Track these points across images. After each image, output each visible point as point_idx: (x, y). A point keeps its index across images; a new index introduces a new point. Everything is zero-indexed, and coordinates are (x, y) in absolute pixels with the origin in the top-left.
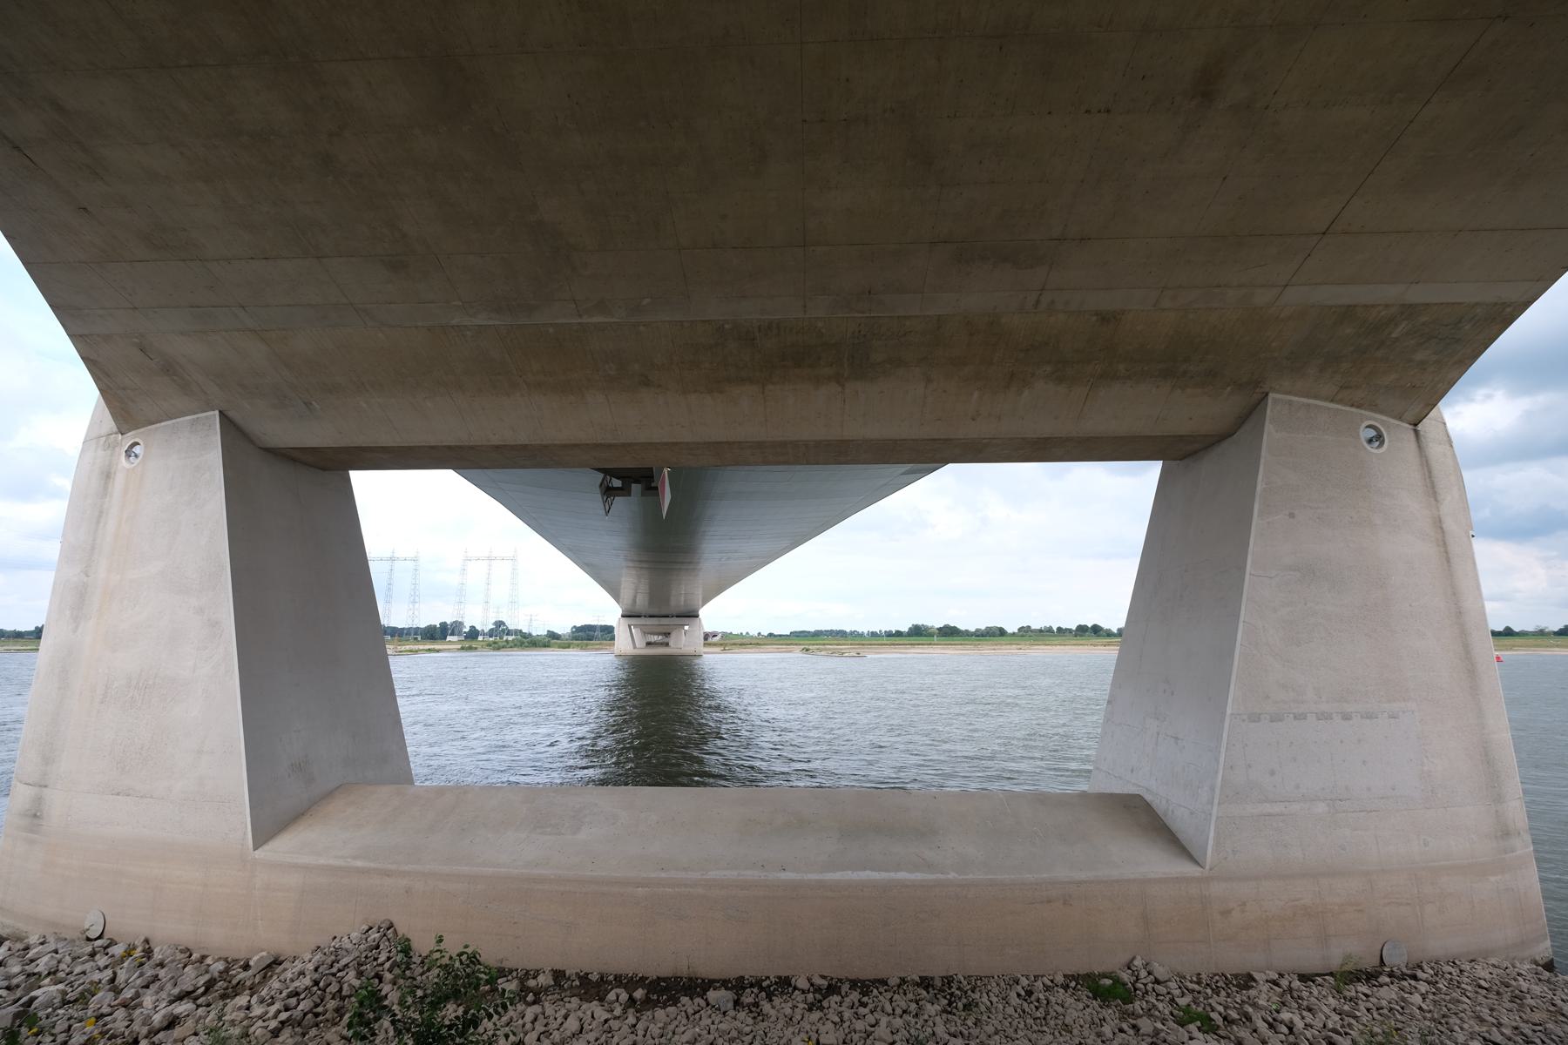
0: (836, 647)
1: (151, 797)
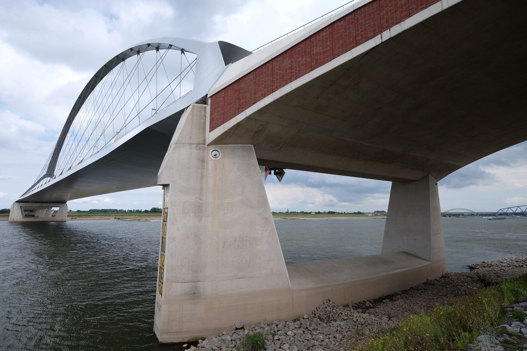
0: (128, 217)
1: (254, 277)
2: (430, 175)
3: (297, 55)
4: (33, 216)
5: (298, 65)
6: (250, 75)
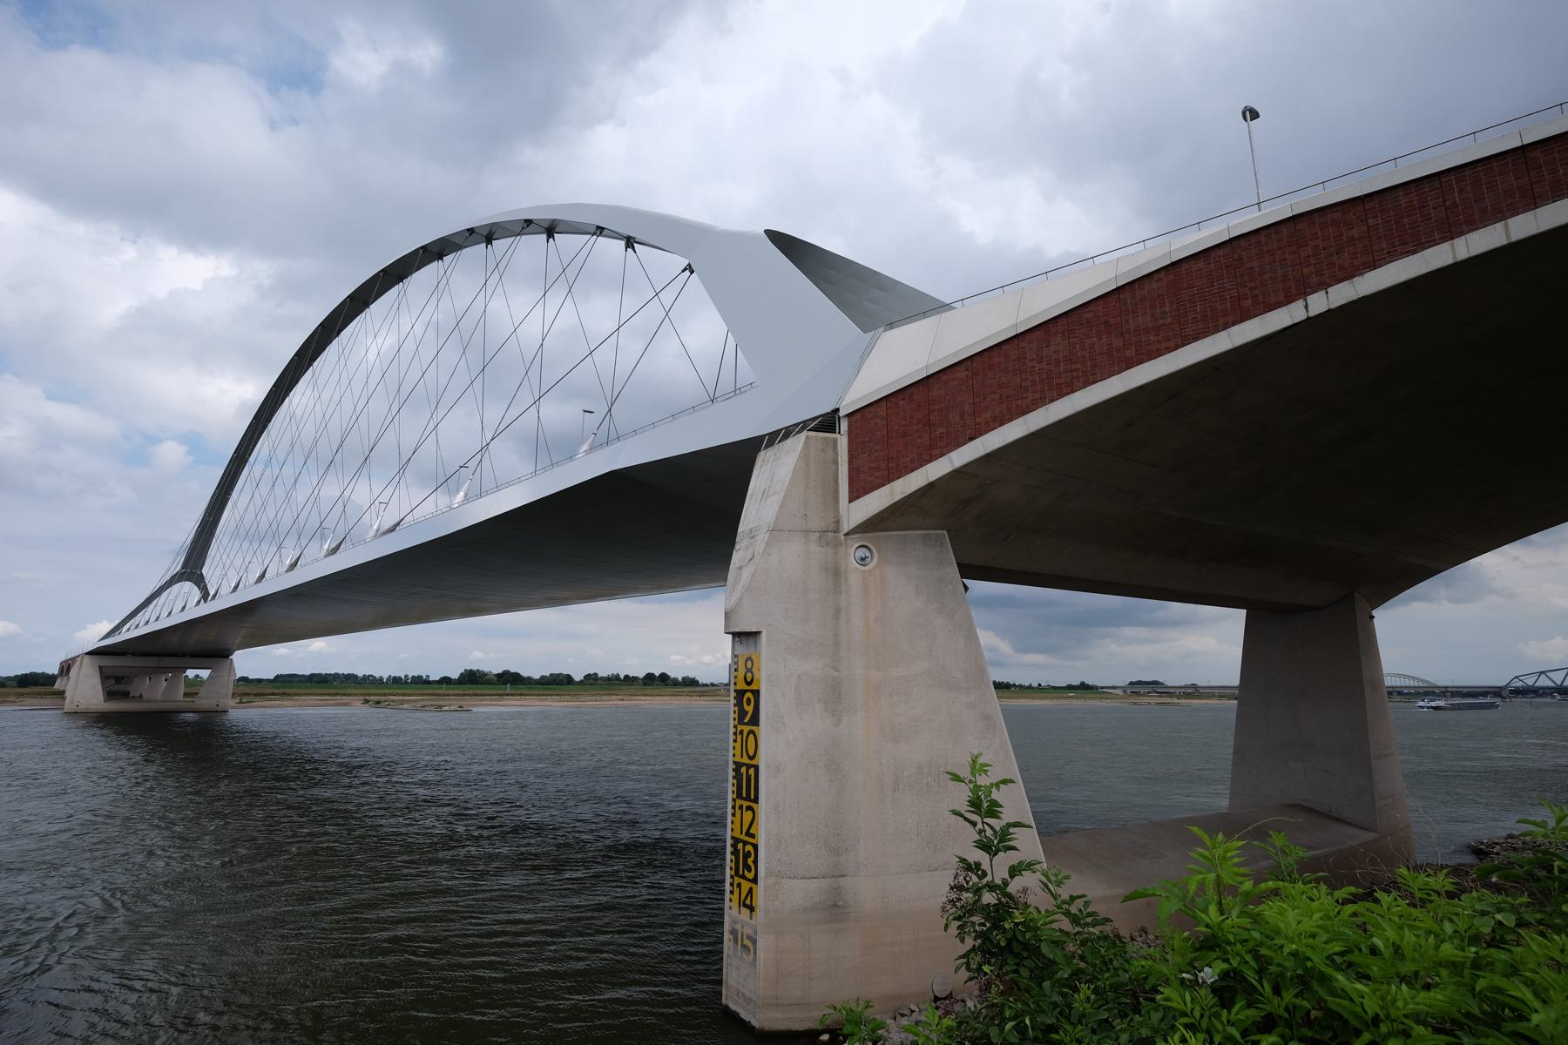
0: (401, 698)
2: (1356, 594)
3: (1084, 330)
4: (125, 695)
5: (1090, 353)
6: (956, 368)
